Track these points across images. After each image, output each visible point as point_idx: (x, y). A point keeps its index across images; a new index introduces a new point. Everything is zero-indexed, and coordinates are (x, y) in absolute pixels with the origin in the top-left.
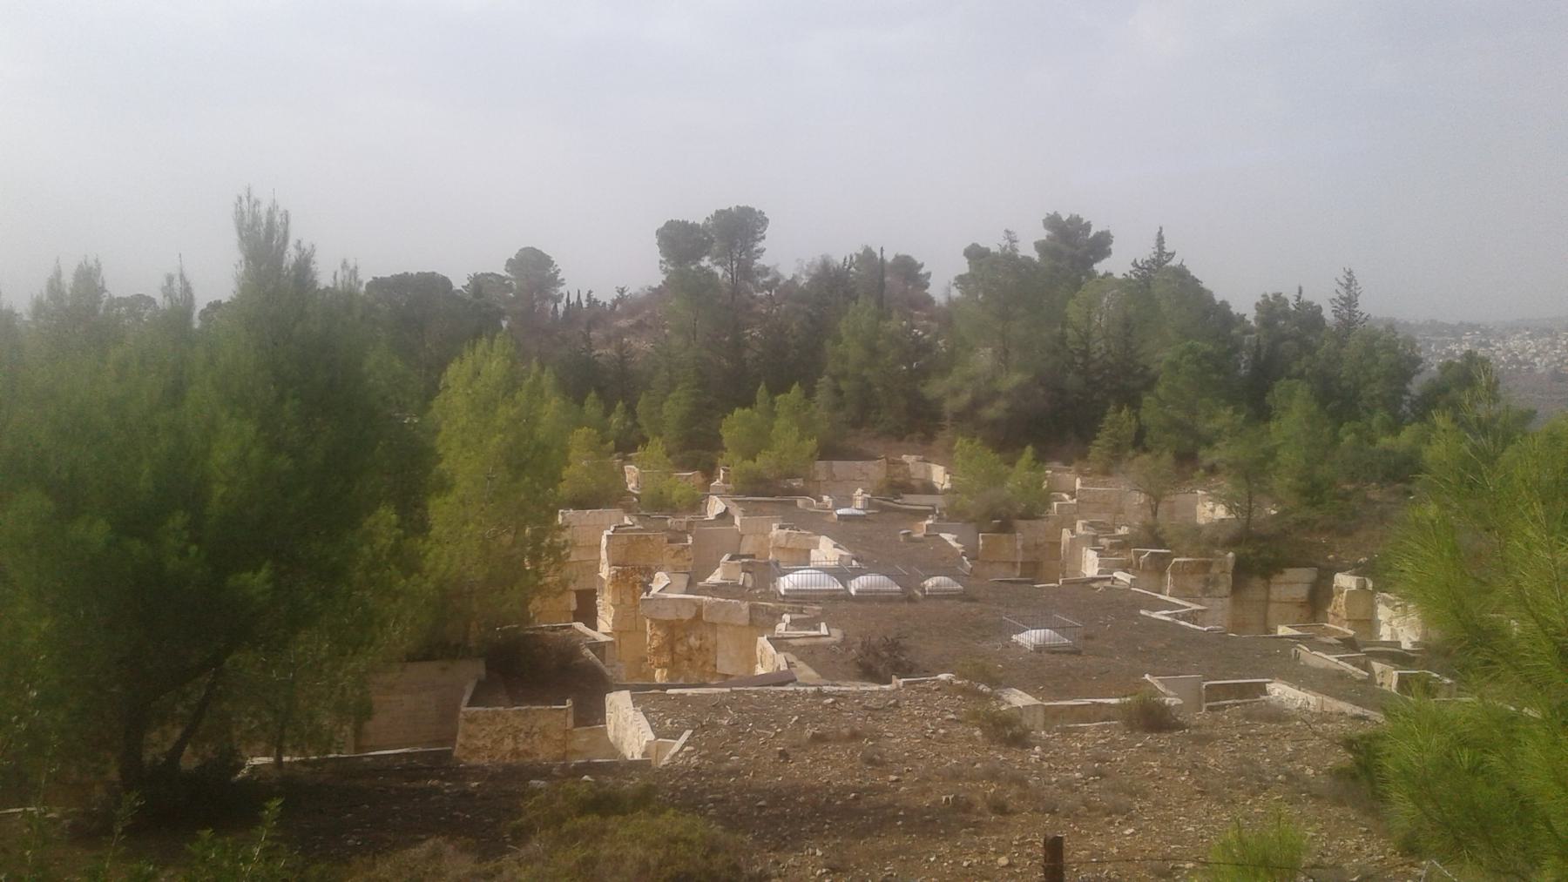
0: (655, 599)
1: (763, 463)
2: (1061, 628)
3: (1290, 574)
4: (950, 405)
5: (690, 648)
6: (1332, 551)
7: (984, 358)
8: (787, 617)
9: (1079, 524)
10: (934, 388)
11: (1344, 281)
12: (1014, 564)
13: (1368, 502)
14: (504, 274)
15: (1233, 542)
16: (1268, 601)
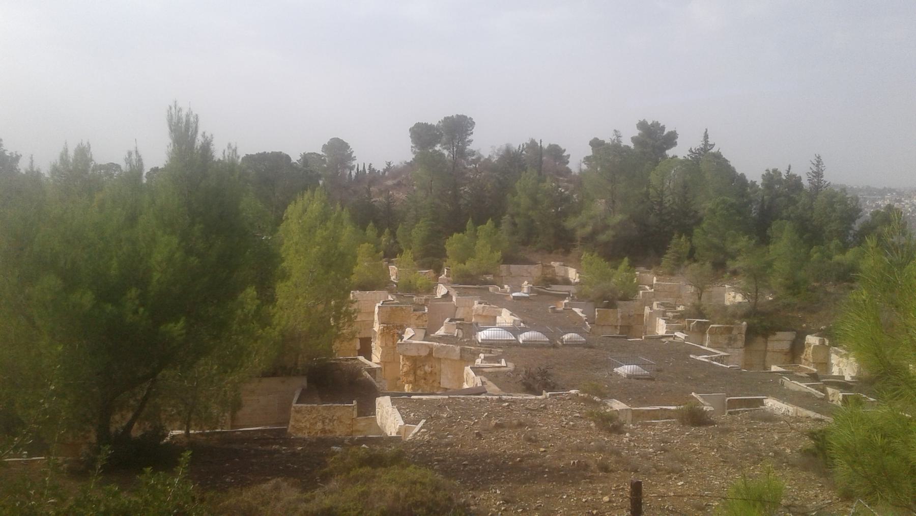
0: (406, 344)
1: (470, 266)
2: (642, 365)
3: (780, 335)
4: (580, 233)
5: (426, 373)
6: (805, 322)
7: (600, 206)
8: (482, 356)
9: (655, 304)
10: (571, 223)
11: (815, 162)
12: (616, 327)
13: (826, 293)
14: (321, 153)
15: (746, 316)
16: (766, 351)
